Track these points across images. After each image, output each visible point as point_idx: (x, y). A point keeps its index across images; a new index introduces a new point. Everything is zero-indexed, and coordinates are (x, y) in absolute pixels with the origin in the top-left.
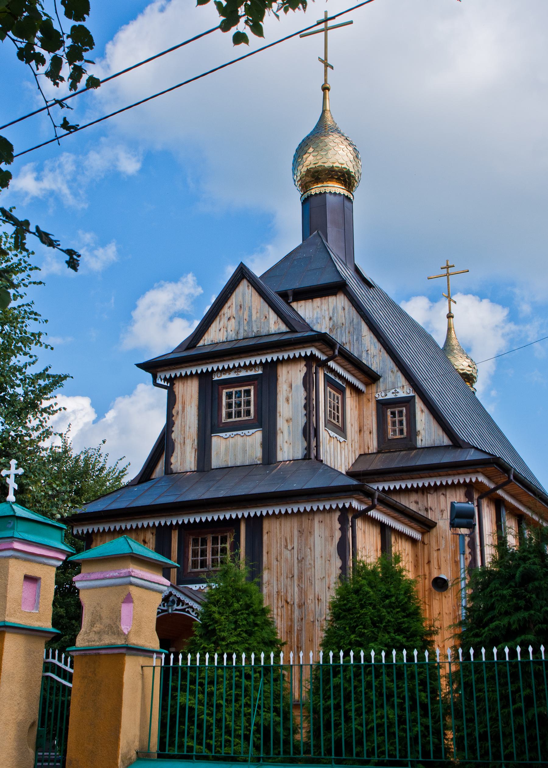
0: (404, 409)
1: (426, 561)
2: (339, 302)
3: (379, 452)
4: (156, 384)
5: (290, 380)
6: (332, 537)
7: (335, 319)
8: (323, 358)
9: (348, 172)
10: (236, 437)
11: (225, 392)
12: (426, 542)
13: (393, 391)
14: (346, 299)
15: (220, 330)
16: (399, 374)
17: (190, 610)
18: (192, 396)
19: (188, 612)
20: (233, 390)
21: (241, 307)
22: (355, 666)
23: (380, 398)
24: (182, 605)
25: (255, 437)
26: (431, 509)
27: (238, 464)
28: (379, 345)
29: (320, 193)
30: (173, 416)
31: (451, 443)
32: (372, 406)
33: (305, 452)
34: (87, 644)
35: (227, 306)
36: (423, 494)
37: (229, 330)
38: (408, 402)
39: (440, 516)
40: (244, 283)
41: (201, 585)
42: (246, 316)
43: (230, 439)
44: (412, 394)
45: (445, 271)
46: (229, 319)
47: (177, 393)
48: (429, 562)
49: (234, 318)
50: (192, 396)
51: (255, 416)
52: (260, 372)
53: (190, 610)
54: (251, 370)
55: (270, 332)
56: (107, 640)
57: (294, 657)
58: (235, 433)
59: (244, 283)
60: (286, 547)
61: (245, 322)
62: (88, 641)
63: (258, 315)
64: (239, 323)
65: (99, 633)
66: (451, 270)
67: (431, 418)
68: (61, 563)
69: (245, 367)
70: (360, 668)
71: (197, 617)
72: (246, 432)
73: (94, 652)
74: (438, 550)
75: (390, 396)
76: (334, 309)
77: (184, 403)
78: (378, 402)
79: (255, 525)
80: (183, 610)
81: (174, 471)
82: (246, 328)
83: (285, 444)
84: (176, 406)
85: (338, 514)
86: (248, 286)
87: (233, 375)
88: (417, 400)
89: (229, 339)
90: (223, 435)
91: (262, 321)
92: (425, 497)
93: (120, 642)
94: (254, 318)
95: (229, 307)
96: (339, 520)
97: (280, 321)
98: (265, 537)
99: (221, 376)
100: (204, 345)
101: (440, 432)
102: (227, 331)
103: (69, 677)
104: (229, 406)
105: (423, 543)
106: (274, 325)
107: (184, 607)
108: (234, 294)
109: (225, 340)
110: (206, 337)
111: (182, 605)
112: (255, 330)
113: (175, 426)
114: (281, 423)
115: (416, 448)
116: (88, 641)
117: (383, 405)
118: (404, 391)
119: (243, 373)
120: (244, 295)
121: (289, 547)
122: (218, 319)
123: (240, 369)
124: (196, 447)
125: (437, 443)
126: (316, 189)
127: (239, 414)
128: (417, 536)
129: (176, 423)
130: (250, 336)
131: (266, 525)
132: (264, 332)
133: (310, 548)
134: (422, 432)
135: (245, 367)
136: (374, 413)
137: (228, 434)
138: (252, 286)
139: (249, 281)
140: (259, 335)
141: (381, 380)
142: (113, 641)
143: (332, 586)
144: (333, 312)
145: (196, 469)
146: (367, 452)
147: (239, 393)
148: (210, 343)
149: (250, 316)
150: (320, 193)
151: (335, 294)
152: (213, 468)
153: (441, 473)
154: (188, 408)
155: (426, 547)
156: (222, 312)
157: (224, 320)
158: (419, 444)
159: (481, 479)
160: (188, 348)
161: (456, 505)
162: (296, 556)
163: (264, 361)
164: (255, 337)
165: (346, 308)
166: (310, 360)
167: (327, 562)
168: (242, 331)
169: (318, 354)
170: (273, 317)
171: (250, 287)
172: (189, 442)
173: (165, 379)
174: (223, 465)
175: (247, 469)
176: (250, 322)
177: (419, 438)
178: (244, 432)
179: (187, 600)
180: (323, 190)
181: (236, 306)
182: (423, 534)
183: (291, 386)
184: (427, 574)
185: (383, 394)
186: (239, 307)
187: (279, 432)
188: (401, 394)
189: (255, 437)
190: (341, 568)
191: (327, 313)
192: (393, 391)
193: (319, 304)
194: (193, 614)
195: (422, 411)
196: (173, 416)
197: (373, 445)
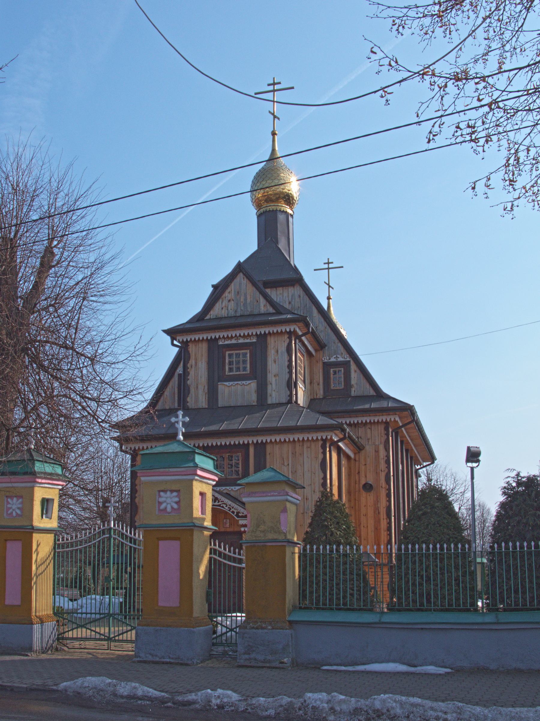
0: (342, 369)
1: (357, 472)
2: (297, 290)
3: (324, 398)
4: (173, 344)
5: (276, 347)
6: (317, 458)
7: (293, 303)
8: (300, 333)
9: (293, 197)
10: (237, 386)
11: (332, 370)
12: (357, 459)
13: (335, 356)
14: (301, 290)
15: (222, 309)
16: (340, 344)
17: (224, 506)
18: (202, 355)
19: (223, 507)
20: (234, 352)
21: (238, 293)
22: (440, 554)
23: (326, 361)
24: (219, 502)
25: (253, 385)
26: (361, 437)
27: (239, 405)
28: (325, 324)
29: (273, 210)
30: (188, 368)
31: (375, 394)
32: (320, 365)
33: (289, 398)
34: (254, 538)
35: (227, 291)
36: (355, 427)
37: (229, 308)
38: (346, 365)
39: (367, 443)
40: (241, 275)
41: (221, 488)
42: (242, 299)
43: (232, 387)
44: (348, 359)
45: (326, 266)
46: (229, 301)
47: (191, 352)
48: (359, 473)
49: (233, 300)
50: (202, 355)
51: (250, 372)
52: (254, 340)
53: (224, 506)
54: (247, 339)
55: (261, 313)
56: (271, 536)
57: (384, 548)
58: (236, 383)
59: (241, 275)
60: (283, 464)
61: (242, 304)
62: (256, 537)
63: (252, 299)
64: (237, 304)
65: (263, 532)
66: (331, 266)
67: (362, 376)
68: (215, 483)
69: (244, 337)
70: (444, 555)
71: (229, 510)
72: (244, 382)
73: (262, 544)
74: (365, 465)
75: (333, 360)
76: (292, 296)
77: (196, 360)
78: (324, 363)
79: (261, 447)
80: (219, 506)
81: (190, 407)
82: (242, 308)
83: (273, 392)
84: (190, 362)
85: (320, 443)
86: (244, 278)
87: (234, 341)
88: (352, 363)
89: (229, 315)
90: (227, 383)
91: (255, 304)
92: (357, 429)
93: (281, 537)
94: (248, 301)
95: (229, 293)
96: (321, 446)
97: (268, 305)
98: (268, 457)
99: (225, 341)
100: (210, 319)
101: (368, 386)
102: (228, 309)
103: (240, 561)
104: (230, 363)
105: (355, 460)
106: (263, 307)
107: (220, 503)
108: (233, 283)
109: (226, 315)
110: (212, 312)
111: (219, 502)
112: (249, 310)
113: (190, 375)
114: (271, 378)
115: (351, 397)
116: (256, 537)
117: (327, 366)
118: (342, 357)
119: (241, 341)
120: (240, 284)
121: (286, 464)
122: (221, 300)
123: (239, 338)
124: (206, 391)
125: (366, 394)
126: (271, 207)
127: (238, 369)
128: (352, 455)
129: (191, 373)
130: (246, 314)
131: (269, 448)
132: (256, 312)
133: (301, 465)
134: (355, 386)
135: (244, 337)
136: (321, 371)
137: (231, 383)
138: (247, 277)
139: (244, 274)
140: (252, 314)
141: (326, 348)
142: (275, 537)
143: (317, 490)
144: (292, 298)
145: (207, 407)
146: (315, 397)
147: (238, 355)
148: (214, 317)
149: (246, 299)
150: (273, 210)
151: (293, 285)
152: (219, 406)
153: (371, 415)
154: (200, 364)
155: (357, 463)
156: (224, 295)
157: (225, 303)
158: (353, 394)
159: (397, 419)
160: (198, 320)
161: (472, 449)
162: (290, 470)
163: (258, 333)
164: (249, 315)
165: (302, 296)
166: (290, 334)
167: (313, 474)
168: (239, 310)
169: (298, 330)
170: (262, 301)
171: (245, 279)
172: (201, 388)
173: (179, 342)
174: (227, 404)
175: (248, 409)
176: (245, 305)
177: (353, 389)
178: (243, 382)
179: (223, 499)
180: (274, 208)
181: (234, 292)
182: (355, 454)
183: (277, 352)
184: (357, 480)
185: (328, 358)
186: (236, 293)
187: (268, 383)
188: (341, 359)
189: (253, 385)
190: (323, 479)
191: (287, 299)
192: (335, 356)
193: (281, 292)
194: (227, 508)
195: (355, 371)
196: (188, 368)
197: (320, 394)
